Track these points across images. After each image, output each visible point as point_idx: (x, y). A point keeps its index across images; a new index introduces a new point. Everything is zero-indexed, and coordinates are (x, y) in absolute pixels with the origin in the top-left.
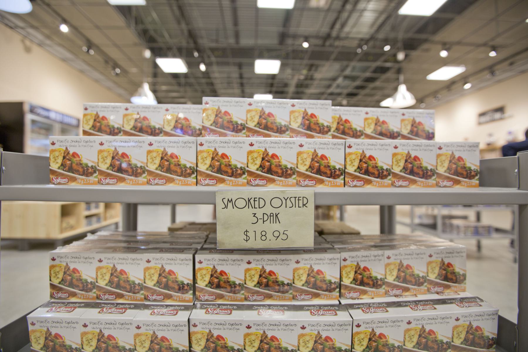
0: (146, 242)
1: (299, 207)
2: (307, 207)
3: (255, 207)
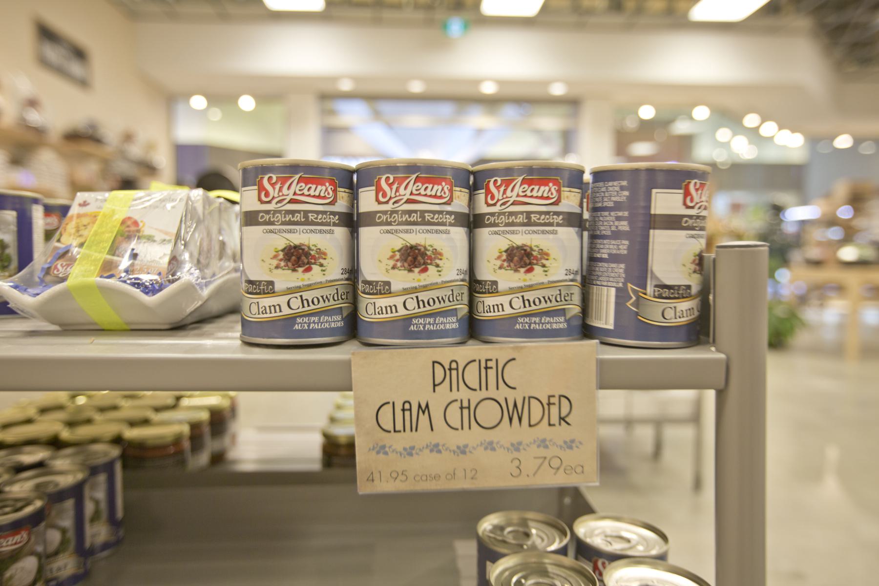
2: (568, 424)
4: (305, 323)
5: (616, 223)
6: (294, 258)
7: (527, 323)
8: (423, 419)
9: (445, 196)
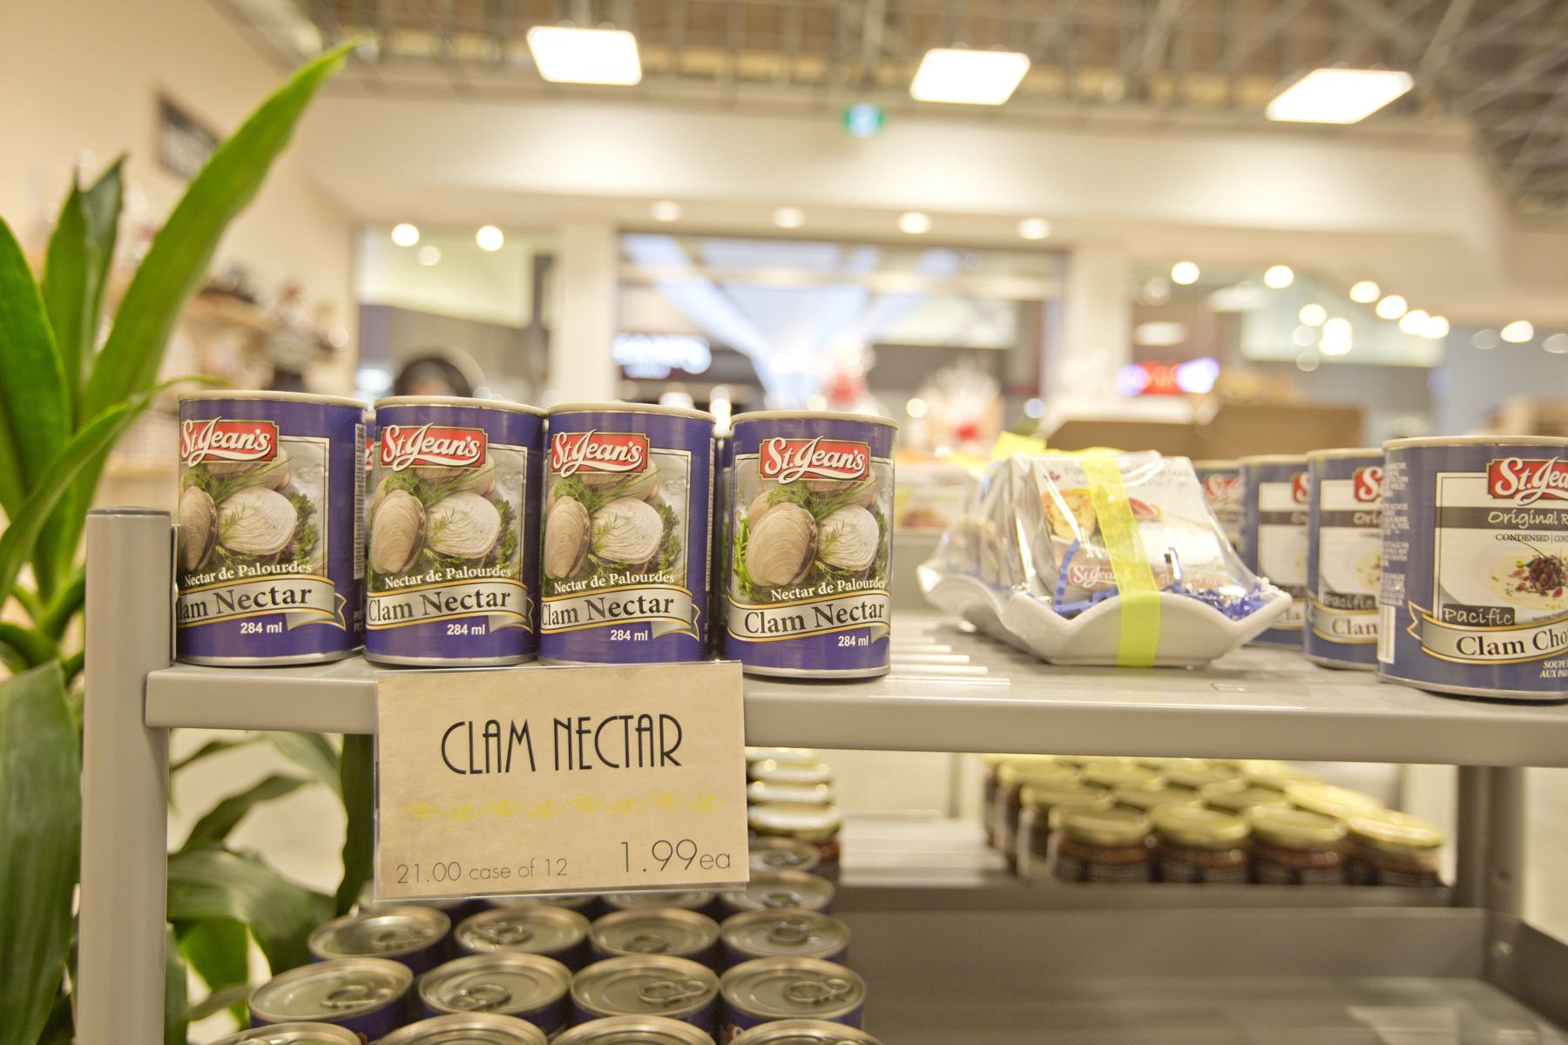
0: (1126, 865)
1: (582, 767)
2: (677, 764)
3: (475, 768)
4: (1554, 669)
5: (1396, 519)
6: (1543, 576)
7: (1554, 669)
8: (520, 750)
9: (856, 468)
